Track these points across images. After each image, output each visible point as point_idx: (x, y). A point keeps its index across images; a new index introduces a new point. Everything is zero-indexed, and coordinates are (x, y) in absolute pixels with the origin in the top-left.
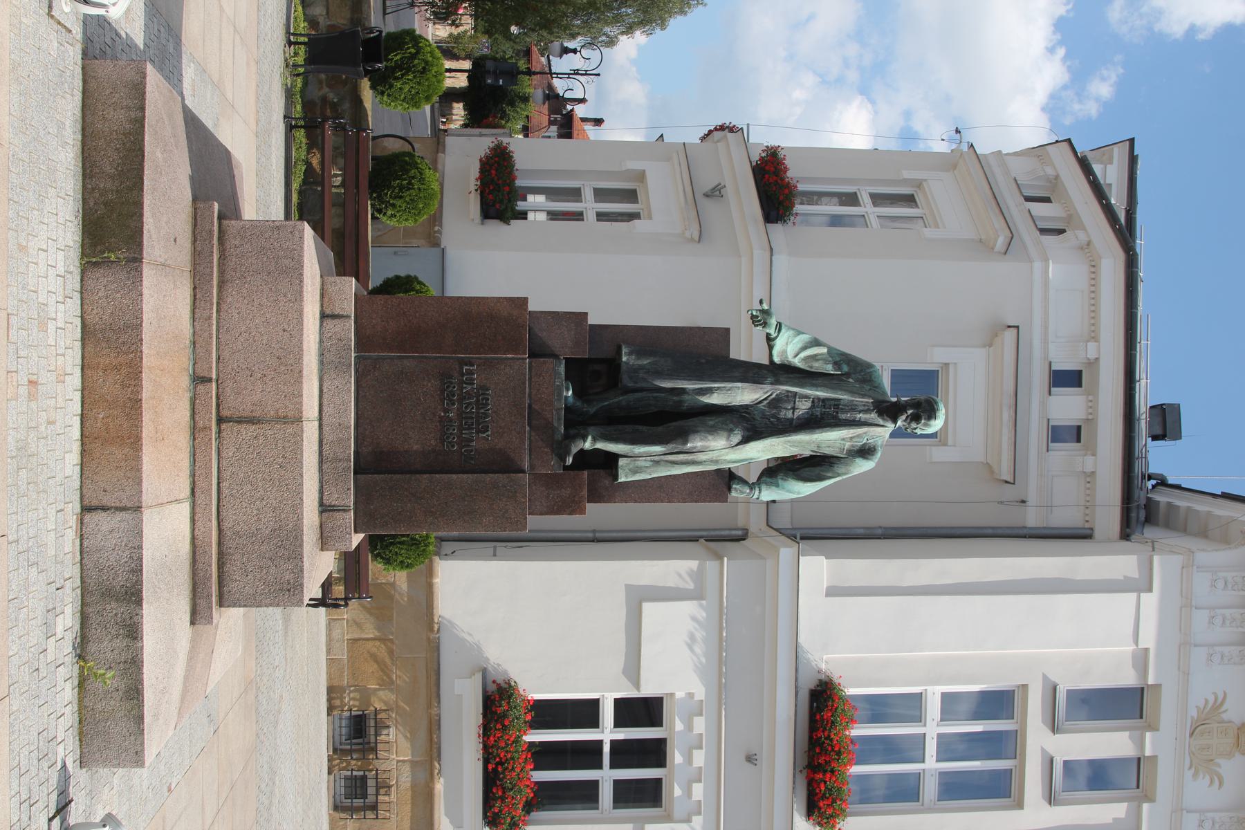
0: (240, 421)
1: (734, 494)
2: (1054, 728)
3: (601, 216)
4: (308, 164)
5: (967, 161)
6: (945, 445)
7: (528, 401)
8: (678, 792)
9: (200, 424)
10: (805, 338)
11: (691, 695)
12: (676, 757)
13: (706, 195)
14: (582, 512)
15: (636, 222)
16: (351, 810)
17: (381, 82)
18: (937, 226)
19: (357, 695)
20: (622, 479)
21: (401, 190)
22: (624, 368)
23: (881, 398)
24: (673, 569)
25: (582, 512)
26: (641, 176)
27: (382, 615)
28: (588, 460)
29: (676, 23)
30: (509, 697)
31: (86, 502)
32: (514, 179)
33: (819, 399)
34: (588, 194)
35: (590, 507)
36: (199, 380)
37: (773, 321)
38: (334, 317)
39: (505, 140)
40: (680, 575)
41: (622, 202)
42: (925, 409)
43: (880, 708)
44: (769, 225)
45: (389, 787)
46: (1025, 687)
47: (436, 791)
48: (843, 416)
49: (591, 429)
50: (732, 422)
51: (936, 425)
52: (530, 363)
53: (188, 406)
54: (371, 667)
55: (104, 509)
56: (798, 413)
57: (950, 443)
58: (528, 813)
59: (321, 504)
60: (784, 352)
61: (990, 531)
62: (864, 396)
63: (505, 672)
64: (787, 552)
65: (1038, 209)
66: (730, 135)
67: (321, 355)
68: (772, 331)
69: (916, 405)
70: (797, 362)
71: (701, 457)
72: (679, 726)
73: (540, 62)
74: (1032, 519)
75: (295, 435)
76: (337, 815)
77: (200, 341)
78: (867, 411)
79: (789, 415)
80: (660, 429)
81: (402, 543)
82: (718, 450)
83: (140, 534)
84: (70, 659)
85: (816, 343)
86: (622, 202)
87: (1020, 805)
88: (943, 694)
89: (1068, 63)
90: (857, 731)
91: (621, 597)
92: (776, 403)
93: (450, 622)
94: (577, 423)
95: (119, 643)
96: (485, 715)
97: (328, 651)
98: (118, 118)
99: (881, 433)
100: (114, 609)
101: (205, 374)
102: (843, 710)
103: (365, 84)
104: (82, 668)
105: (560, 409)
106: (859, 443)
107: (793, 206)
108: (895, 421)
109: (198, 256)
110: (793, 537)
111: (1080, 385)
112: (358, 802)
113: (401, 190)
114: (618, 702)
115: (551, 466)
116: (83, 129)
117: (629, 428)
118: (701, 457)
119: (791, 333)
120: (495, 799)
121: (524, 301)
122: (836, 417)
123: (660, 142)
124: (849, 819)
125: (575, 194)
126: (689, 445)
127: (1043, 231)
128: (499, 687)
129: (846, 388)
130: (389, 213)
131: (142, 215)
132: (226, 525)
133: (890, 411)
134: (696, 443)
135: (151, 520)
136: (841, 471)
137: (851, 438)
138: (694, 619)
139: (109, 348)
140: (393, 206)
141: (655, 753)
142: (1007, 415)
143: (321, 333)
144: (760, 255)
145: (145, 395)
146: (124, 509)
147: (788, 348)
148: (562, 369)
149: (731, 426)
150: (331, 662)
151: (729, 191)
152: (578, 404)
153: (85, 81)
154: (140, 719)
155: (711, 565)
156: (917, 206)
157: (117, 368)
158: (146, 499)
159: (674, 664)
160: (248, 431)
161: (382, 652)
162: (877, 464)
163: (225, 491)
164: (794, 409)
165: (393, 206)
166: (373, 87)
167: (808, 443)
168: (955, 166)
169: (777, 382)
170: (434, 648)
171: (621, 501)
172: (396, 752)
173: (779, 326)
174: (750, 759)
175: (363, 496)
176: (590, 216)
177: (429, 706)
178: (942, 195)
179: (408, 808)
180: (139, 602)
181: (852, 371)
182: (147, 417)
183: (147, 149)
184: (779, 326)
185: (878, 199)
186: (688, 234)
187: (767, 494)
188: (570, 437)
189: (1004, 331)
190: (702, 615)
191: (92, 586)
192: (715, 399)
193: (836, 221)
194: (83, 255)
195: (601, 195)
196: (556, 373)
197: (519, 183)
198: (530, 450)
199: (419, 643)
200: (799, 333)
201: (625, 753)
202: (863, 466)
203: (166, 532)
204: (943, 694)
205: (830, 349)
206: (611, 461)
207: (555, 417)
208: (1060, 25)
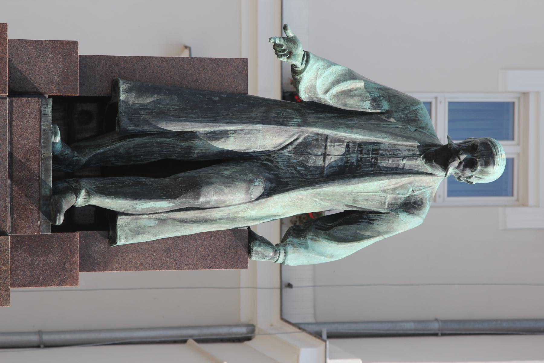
1: (254, 257)
6: (525, 204)
7: (8, 149)
10: (338, 70)
20: (121, 242)
22: (122, 108)
23: (428, 141)
25: (75, 281)
28: (77, 220)
33: (354, 143)
35: (84, 277)
37: (299, 51)
42: (479, 154)
48: (383, 163)
50: (252, 171)
51: (495, 172)
52: (11, 103)
56: (330, 160)
57: (531, 201)
60: (313, 87)
62: (408, 138)
68: (298, 62)
69: (471, 148)
70: (328, 99)
71: (215, 214)
78: (412, 157)
79: (320, 162)
80: (166, 181)
82: (236, 205)
85: (351, 76)
92: (303, 148)
94: (67, 175)
99: (432, 183)
105: (48, 158)
106: (403, 196)
108: (445, 167)
110: (318, 335)
115: (36, 226)
117: (129, 180)
119: (321, 64)
122: (374, 165)
126: (202, 200)
133: (439, 156)
134: (209, 196)
136: (381, 229)
137: (394, 190)
147: (316, 83)
148: (49, 110)
149: (251, 176)
152: (68, 151)
162: (425, 220)
164: (325, 155)
167: (342, 196)
169: (305, 123)
171: (119, 269)
173: (307, 56)
181: (394, 109)
184: (307, 56)
187: (296, 258)
188: (59, 192)
196: (42, 115)
198: (12, 208)
200: (330, 64)
202: (408, 223)
205: (367, 83)
206: (106, 221)
207: (42, 168)
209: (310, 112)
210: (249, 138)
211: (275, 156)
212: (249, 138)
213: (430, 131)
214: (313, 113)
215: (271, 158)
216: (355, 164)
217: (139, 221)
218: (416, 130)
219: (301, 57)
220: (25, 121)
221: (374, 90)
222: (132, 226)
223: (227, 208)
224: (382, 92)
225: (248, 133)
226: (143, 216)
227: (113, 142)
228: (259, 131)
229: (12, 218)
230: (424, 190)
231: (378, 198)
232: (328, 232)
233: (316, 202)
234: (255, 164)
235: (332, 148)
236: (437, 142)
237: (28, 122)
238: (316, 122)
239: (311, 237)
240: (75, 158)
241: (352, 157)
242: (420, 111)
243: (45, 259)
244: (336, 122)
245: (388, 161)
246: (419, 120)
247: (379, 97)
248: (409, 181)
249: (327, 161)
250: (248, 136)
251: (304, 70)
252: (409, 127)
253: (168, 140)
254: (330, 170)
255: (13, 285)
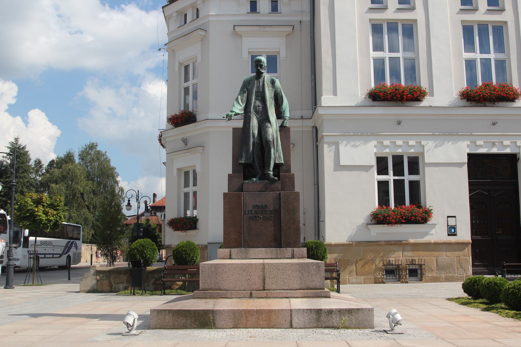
0: (264, 283)
1: (287, 125)
2: (386, 8)
3: (195, 184)
4: (177, 289)
5: (171, 46)
8: (412, 150)
9: (265, 295)
10: (235, 103)
11: (375, 146)
12: (399, 151)
13: (186, 145)
14: (293, 174)
15: (197, 171)
16: (422, 274)
17: (148, 262)
18: (196, 57)
19: (378, 273)
20: (283, 162)
21: (187, 254)
22: (246, 162)
24: (327, 154)
26: (179, 170)
27: (346, 263)
29: (113, 164)
30: (377, 214)
31: (289, 327)
32: (181, 218)
34: (186, 190)
35: (292, 172)
36: (251, 296)
37: (230, 113)
38: (230, 255)
39: (166, 222)
40: (330, 151)
41: (188, 177)
43: (379, 74)
44: (197, 121)
45: (412, 260)
46: (370, 20)
47: (414, 242)
48: (261, 90)
49: (266, 172)
53: (259, 300)
54: (367, 267)
55: (291, 321)
58: (422, 207)
59: (291, 258)
60: (240, 110)
61: (312, 34)
62: (254, 83)
63: (367, 216)
64: (320, 111)
65: (189, 19)
66: (163, 136)
67: (243, 259)
68: (233, 114)
69: (257, 66)
70: (243, 105)
71: (275, 136)
72: (387, 150)
73: (130, 220)
74: (307, 18)
75: (268, 265)
76: (424, 280)
77: (238, 296)
78: (259, 82)
79: (261, 108)
81: (317, 252)
82: (273, 129)
83: (299, 310)
84: (338, 330)
85: (237, 100)
86: (188, 177)
87: (416, 21)
88: (374, 51)
89: (127, 3)
90: (388, 83)
91: (338, 173)
92: (257, 112)
93: (349, 237)
94: (264, 176)
95: (334, 316)
96: (384, 224)
97: (361, 283)
98: (168, 318)
100: (323, 318)
101: (249, 294)
102: (380, 88)
103: (149, 268)
104: (342, 328)
105: (260, 182)
106: (270, 84)
107: (190, 112)
109: (211, 297)
110: (315, 109)
111: (256, 1)
112: (419, 271)
113: (187, 254)
114: (378, 174)
116: (172, 329)
118: (275, 136)
120: (416, 219)
121: (225, 194)
122: (261, 92)
123: (166, 164)
124: (422, 85)
125: (186, 195)
127: (198, 17)
128: (374, 218)
129: (252, 89)
130: (195, 258)
131: (199, 310)
132: (298, 287)
133: (259, 75)
134: (270, 138)
135: (293, 307)
136: (279, 90)
138: (346, 145)
139: (240, 320)
140: (192, 257)
141: (398, 160)
142: (268, 29)
143: (236, 259)
144: (209, 124)
145: (255, 308)
146: (291, 315)
147: (239, 109)
148: (246, 181)
150: (365, 283)
151: (185, 136)
153: (157, 329)
154: (358, 310)
155: (326, 139)
156: (189, 65)
157: (247, 317)
158: (289, 308)
159: (365, 153)
160: (267, 280)
161: (361, 263)
163: (287, 288)
164: (259, 106)
165: (192, 257)
166: (149, 265)
168: (173, 51)
170: (359, 243)
172: (399, 257)
174: (399, 123)
175: (288, 245)
176: (195, 189)
177: (381, 245)
178: (184, 55)
179: (420, 252)
180: (321, 310)
181: (246, 87)
182: (262, 308)
183: (178, 309)
184: (232, 111)
185: (186, 80)
186: (201, 151)
187: (287, 114)
189: (236, 31)
190: (345, 142)
191: (315, 325)
192: (256, 132)
193: (195, 98)
194: (211, 328)
195: (187, 185)
196: (248, 183)
197: (182, 216)
199: (357, 251)
200: (234, 105)
201: (398, 171)
202: (278, 83)
203: (299, 304)
204: (374, 51)
205: (239, 95)
206: (277, 166)
208: (112, 7)
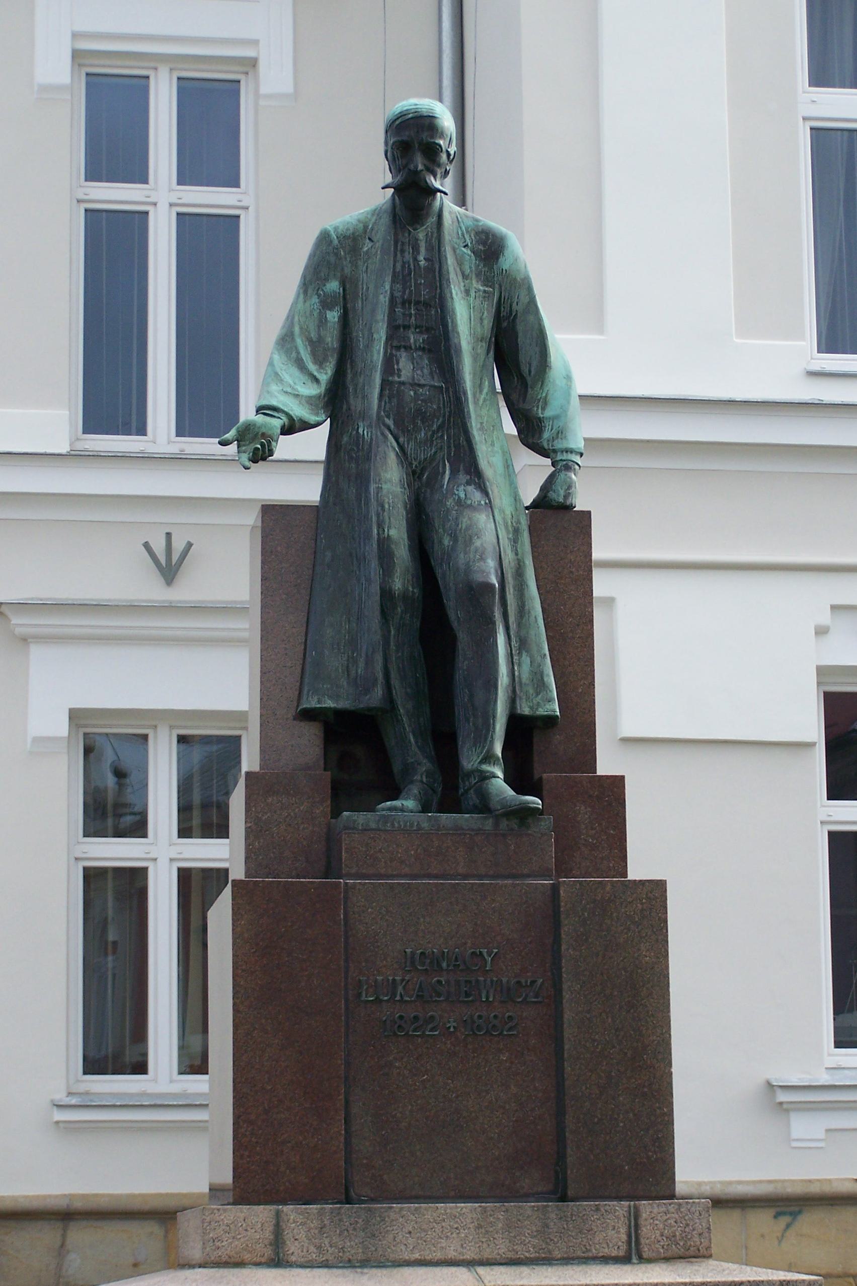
6: (253, 63)
68: (276, 423)
126: (494, 581)
137: (465, 277)
148: (361, 818)
188: (484, 806)
209: (345, 407)
210: (389, 503)
211: (415, 463)
212: (389, 503)
213: (369, 216)
214: (348, 403)
215: (418, 471)
216: (426, 337)
217: (524, 681)
218: (370, 239)
219: (268, 419)
220: (380, 856)
221: (308, 304)
222: (531, 691)
223: (501, 541)
224: (310, 291)
225: (383, 506)
226: (516, 673)
227: (398, 721)
228: (379, 489)
229: (528, 876)
230: (464, 228)
231: (478, 302)
232: (529, 383)
233: (485, 400)
234: (428, 495)
235: (403, 372)
236: (389, 205)
237: (380, 851)
238: (363, 398)
239: (540, 410)
240: (424, 780)
241: (415, 341)
242: (340, 231)
243: (583, 826)
244: (360, 365)
245: (421, 284)
246: (353, 234)
247: (319, 296)
248: (452, 253)
249: (422, 382)
250: (387, 506)
251: (287, 414)
252: (365, 249)
253: (393, 632)
254: (436, 377)
255: (625, 875)
